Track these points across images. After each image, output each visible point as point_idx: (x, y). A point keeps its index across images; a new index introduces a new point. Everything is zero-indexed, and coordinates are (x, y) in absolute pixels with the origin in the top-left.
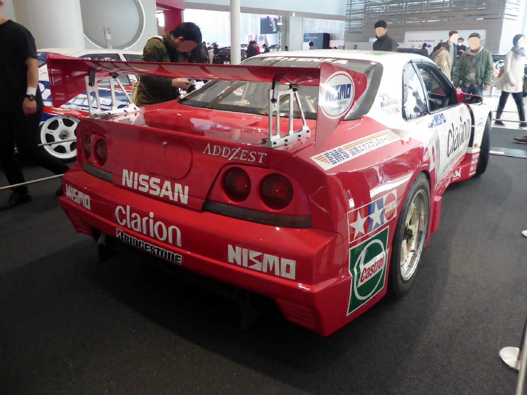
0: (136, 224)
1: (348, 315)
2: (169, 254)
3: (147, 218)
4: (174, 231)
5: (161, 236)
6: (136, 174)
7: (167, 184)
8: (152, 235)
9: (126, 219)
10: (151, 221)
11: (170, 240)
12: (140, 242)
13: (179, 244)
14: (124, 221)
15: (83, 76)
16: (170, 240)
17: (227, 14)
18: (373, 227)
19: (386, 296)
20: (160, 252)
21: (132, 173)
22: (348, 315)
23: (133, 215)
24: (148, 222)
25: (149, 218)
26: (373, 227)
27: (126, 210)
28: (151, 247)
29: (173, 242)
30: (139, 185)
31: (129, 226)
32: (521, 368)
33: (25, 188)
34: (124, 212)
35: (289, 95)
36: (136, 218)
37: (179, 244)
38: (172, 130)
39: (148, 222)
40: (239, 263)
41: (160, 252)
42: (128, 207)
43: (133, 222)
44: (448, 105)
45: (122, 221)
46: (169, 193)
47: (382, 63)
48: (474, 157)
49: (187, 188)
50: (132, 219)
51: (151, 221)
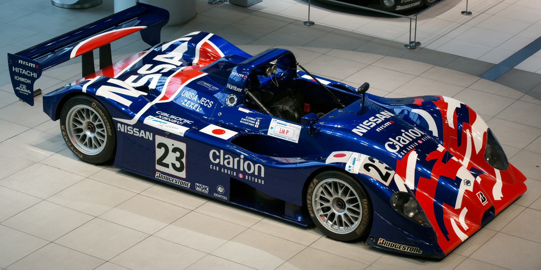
0: (403, 141)
3: (237, 159)
4: (259, 168)
10: (242, 161)
11: (256, 173)
13: (263, 175)
16: (256, 173)
19: (494, 66)
24: (239, 162)
25: (240, 158)
32: (319, 188)
33: (183, 82)
34: (391, 143)
35: (386, 182)
36: (229, 158)
37: (263, 175)
39: (239, 162)
42: (390, 139)
46: (144, 135)
47: (370, 86)
50: (399, 141)
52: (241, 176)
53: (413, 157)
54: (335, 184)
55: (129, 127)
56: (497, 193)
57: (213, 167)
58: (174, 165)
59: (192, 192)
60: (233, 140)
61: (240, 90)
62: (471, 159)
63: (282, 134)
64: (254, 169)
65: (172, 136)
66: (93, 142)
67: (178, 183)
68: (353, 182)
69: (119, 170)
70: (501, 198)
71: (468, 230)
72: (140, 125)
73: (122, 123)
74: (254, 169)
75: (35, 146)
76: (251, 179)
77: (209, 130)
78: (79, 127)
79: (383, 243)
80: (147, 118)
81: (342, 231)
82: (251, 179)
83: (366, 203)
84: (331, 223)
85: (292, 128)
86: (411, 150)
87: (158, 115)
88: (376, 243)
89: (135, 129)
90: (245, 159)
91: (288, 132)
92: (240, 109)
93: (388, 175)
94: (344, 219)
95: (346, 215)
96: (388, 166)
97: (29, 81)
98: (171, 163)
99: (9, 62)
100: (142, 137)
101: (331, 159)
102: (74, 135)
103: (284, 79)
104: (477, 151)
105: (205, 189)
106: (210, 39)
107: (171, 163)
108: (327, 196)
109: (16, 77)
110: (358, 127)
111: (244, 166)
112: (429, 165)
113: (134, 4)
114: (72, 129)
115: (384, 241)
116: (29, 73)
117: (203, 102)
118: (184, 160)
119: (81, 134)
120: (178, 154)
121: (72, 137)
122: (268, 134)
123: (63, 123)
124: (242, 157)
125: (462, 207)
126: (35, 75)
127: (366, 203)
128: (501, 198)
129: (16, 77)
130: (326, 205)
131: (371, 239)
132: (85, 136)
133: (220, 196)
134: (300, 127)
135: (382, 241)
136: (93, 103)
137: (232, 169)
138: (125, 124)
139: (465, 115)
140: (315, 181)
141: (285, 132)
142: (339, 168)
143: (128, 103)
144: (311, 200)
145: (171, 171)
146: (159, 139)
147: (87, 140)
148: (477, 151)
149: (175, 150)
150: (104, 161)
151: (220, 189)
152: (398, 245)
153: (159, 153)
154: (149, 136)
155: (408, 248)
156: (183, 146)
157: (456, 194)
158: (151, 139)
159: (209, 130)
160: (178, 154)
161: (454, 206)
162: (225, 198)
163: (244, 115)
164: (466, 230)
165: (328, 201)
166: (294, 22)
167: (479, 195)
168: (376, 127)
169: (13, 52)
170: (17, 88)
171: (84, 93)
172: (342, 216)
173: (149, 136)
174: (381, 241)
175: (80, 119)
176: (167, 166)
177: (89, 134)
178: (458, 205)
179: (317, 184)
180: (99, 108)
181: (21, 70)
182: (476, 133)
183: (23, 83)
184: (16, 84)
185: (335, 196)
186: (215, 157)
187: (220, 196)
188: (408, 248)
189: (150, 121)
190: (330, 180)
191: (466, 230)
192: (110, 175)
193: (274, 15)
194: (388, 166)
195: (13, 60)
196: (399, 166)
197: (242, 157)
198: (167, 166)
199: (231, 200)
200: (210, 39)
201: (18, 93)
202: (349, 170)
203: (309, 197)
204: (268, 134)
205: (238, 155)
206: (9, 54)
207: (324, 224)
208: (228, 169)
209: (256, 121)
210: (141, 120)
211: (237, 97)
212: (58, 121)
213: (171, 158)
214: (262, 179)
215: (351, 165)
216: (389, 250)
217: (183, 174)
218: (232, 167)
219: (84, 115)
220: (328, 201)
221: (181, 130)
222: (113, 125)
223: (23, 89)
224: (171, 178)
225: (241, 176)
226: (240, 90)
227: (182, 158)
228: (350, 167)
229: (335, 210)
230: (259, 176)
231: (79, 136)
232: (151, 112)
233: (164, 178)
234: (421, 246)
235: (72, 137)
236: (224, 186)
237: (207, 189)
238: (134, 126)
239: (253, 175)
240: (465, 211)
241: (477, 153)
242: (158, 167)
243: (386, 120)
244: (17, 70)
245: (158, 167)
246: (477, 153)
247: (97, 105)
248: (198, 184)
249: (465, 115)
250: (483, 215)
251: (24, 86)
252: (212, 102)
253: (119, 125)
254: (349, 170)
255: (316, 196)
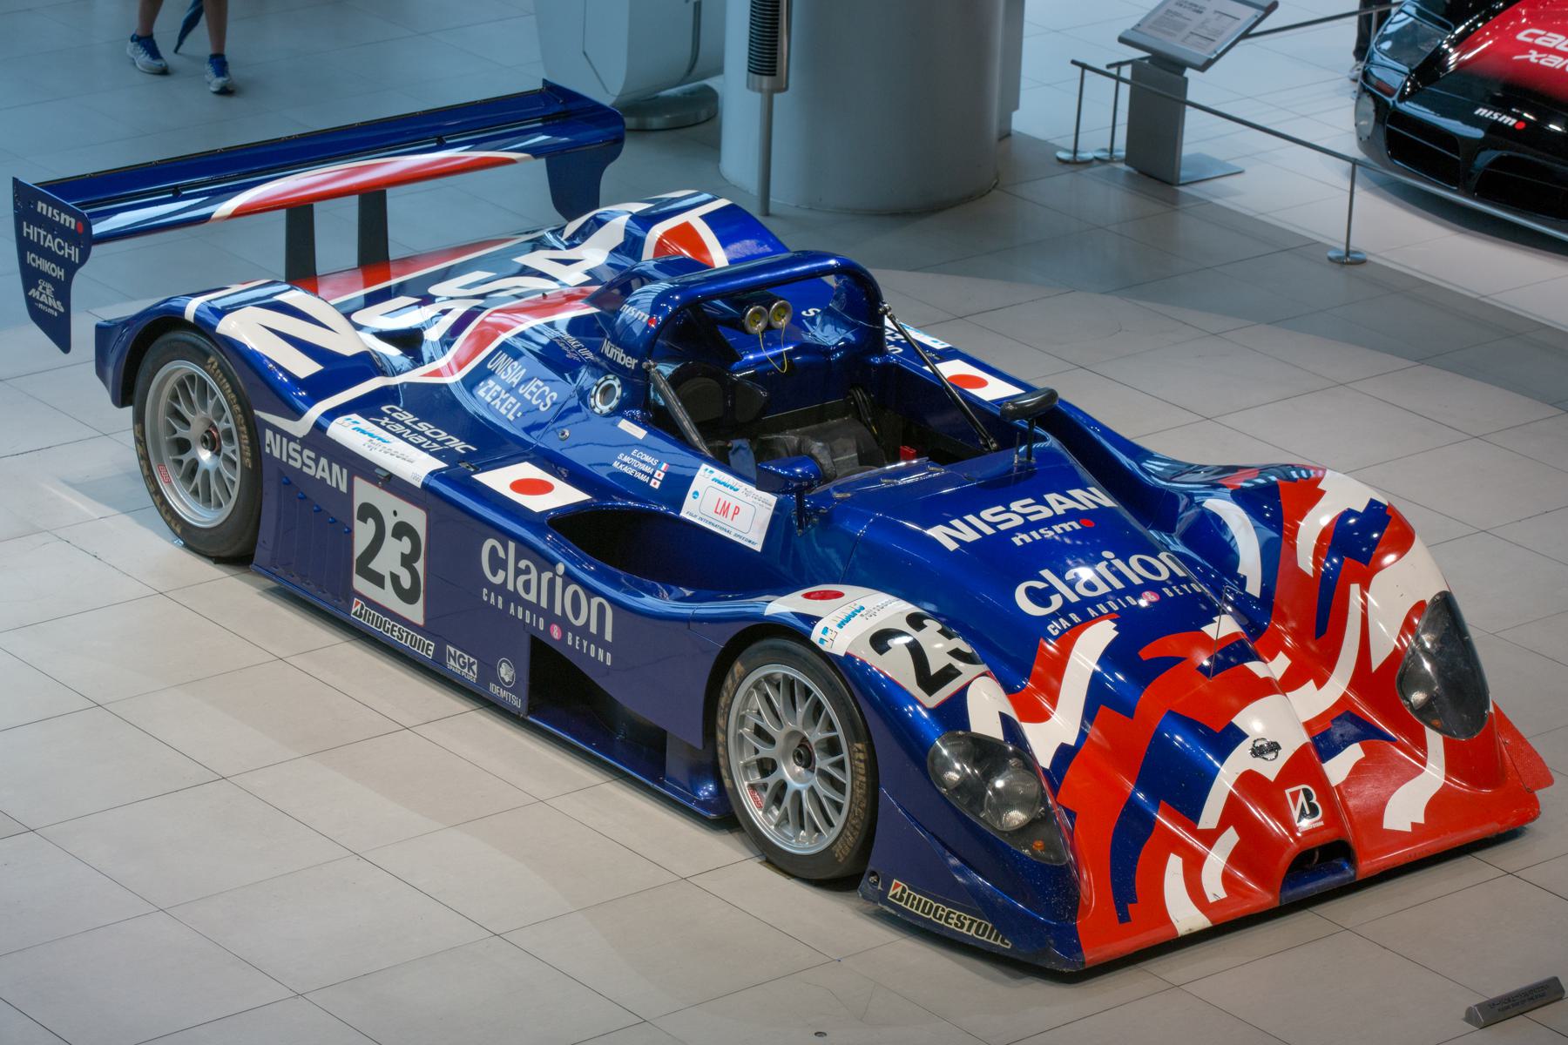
0: (527, 585)
5: (577, 615)
8: (558, 611)
9: (506, 570)
10: (559, 581)
11: (593, 629)
13: (608, 637)
14: (501, 574)
23: (523, 564)
24: (552, 583)
25: (555, 574)
27: (1045, 581)
29: (1263, 590)
31: (510, 587)
34: (501, 554)
36: (527, 571)
37: (608, 637)
38: (389, 288)
39: (552, 583)
42: (1046, 573)
43: (522, 578)
44: (1313, 851)
45: (494, 574)
46: (326, 475)
48: (1289, 850)
50: (518, 572)
51: (559, 581)
52: (556, 632)
53: (1101, 634)
54: (791, 683)
55: (292, 445)
56: (1406, 808)
57: (489, 595)
58: (395, 579)
59: (434, 672)
60: (563, 522)
61: (630, 362)
62: (1353, 685)
63: (720, 518)
64: (589, 612)
65: (391, 483)
66: (214, 487)
67: (397, 634)
68: (830, 683)
69: (270, 584)
70: (1414, 825)
71: (1220, 903)
72: (318, 439)
73: (276, 430)
74: (589, 612)
75: (72, 485)
76: (581, 645)
77: (499, 480)
78: (182, 433)
79: (901, 899)
80: (341, 419)
81: (801, 844)
82: (581, 645)
83: (861, 756)
84: (776, 813)
85: (749, 499)
86: (1101, 616)
87: (382, 415)
88: (882, 897)
89: (306, 452)
90: (569, 577)
91: (737, 511)
92: (625, 425)
93: (949, 674)
94: (808, 806)
95: (812, 790)
96: (966, 648)
97: (60, 273)
98: (389, 567)
99: (16, 207)
100: (323, 480)
101: (780, 606)
102: (168, 458)
103: (839, 360)
104: (1377, 660)
105: (471, 665)
106: (706, 218)
107: (389, 567)
108: (768, 725)
109: (30, 257)
110: (956, 522)
111: (564, 598)
112: (1143, 673)
113: (539, 86)
114: (165, 438)
115: (904, 890)
116: (61, 248)
117: (532, 394)
118: (420, 565)
119: (186, 458)
120: (406, 545)
121: (161, 464)
122: (683, 514)
123: (139, 418)
124: (561, 568)
125: (1223, 825)
126: (73, 253)
127: (861, 756)
128: (1414, 825)
129: (30, 257)
130: (766, 752)
131: (873, 879)
132: (195, 464)
133: (504, 694)
134: (772, 499)
135: (899, 890)
136: (211, 359)
137: (534, 608)
138: (284, 434)
139: (1367, 538)
140: (738, 667)
141: (731, 512)
142: (796, 632)
143: (305, 367)
144: (726, 733)
145: (387, 597)
146: (364, 492)
147: (198, 479)
148: (1377, 660)
149: (402, 530)
150: (232, 549)
151: (505, 672)
152: (943, 910)
153: (363, 534)
154: (336, 477)
155: (973, 922)
156: (417, 518)
157: (1209, 777)
158: (343, 488)
159: (499, 480)
160: (406, 545)
161: (1197, 818)
162: (517, 703)
163: (629, 444)
164: (1212, 899)
165: (770, 741)
166: (1298, 247)
167: (1295, 796)
168: (1013, 531)
169: (29, 180)
170: (33, 292)
171: (188, 323)
172: (805, 795)
173: (336, 477)
174: (897, 888)
175: (183, 408)
176: (378, 580)
177: (205, 456)
178: (1210, 816)
179: (742, 679)
180: (225, 375)
181: (43, 233)
182: (1386, 604)
183: (47, 277)
184: (30, 278)
185: (790, 726)
186: (498, 564)
187: (504, 694)
188: (973, 922)
189: (349, 432)
190: (779, 670)
191: (1212, 899)
192: (240, 594)
193: (1251, 218)
194: (966, 648)
195: (24, 196)
196: (1023, 662)
197: (561, 568)
198: (378, 580)
199: (532, 710)
200: (706, 218)
201: (31, 303)
202: (822, 640)
203: (721, 722)
204: (683, 514)
205: (553, 563)
206: (15, 181)
207: (757, 815)
208: (527, 605)
209: (656, 468)
210: (319, 428)
211: (624, 385)
212: (129, 410)
213: (388, 560)
214: (606, 647)
215: (833, 626)
216: (918, 923)
217: (415, 612)
218: (534, 600)
219: (194, 396)
220: (770, 741)
221: (417, 466)
222: (255, 430)
223: (45, 295)
224: (390, 623)
225: (556, 632)
226: (630, 362)
227: (416, 560)
228: (826, 630)
229: (790, 773)
230: (598, 640)
231: (180, 462)
232: (368, 406)
233: (371, 621)
234: (1001, 919)
235: (161, 464)
236: (515, 664)
237: (475, 668)
238: (305, 442)
239: (583, 631)
240: (1230, 838)
241: (1375, 667)
242: (360, 584)
243: (1071, 514)
244: (32, 232)
245: (360, 584)
246: (1375, 667)
247: (219, 367)
248: (452, 650)
249: (1367, 538)
250: (1314, 872)
251: (48, 286)
252: (555, 395)
253: (269, 434)
254: (822, 640)
255: (742, 720)
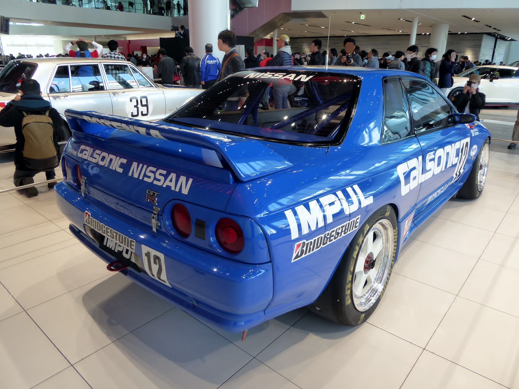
1: (292, 261)
2: (125, 238)
6: (145, 166)
7: (173, 176)
12: (102, 225)
15: (227, 147)
17: (321, 199)
18: (293, 258)
20: (118, 236)
21: (141, 165)
22: (292, 261)
26: (293, 258)
28: (111, 230)
30: (145, 175)
40: (301, 209)
41: (118, 236)
46: (172, 185)
49: (191, 181)
